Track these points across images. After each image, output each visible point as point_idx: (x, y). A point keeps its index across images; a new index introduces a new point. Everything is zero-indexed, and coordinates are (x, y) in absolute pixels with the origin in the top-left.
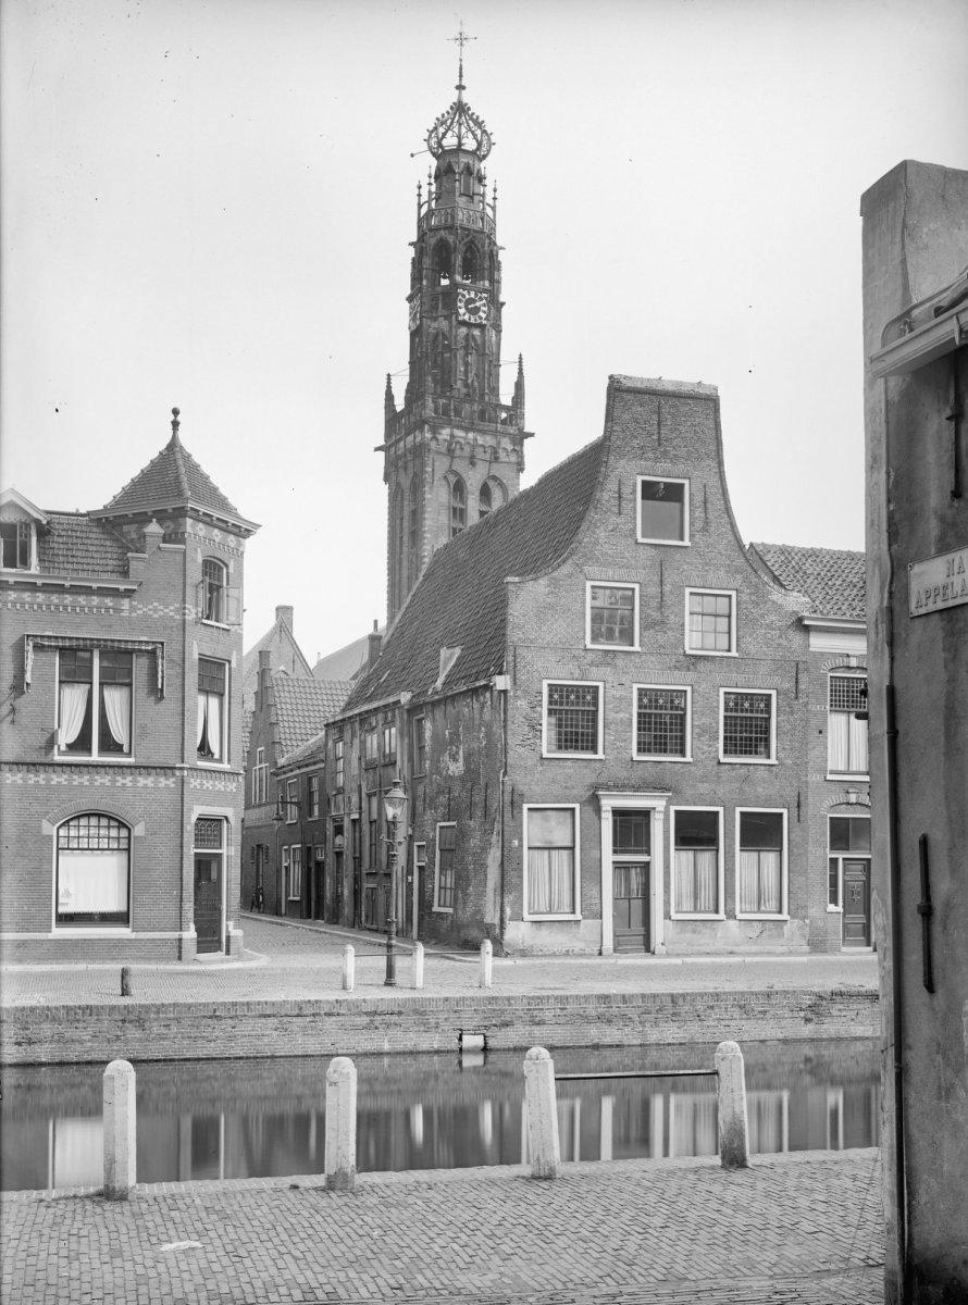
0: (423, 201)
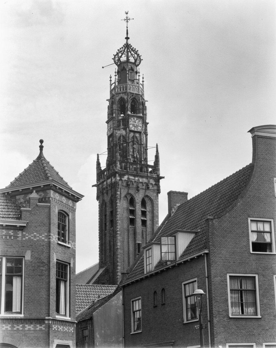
0: (112, 82)
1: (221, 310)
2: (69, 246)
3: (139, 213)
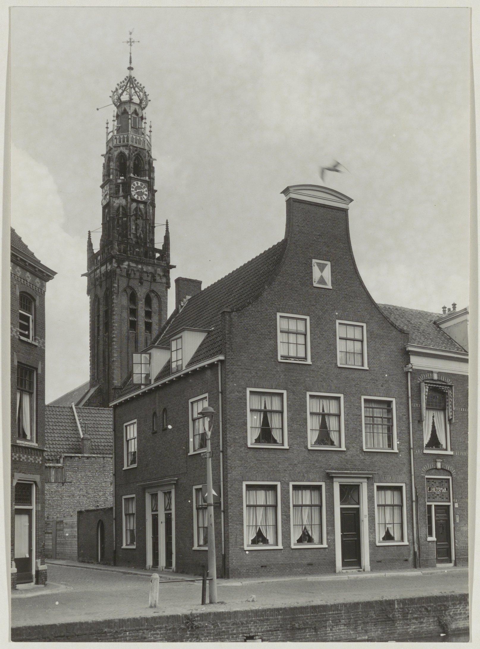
1: (237, 437)
2: (37, 344)
3: (141, 313)
